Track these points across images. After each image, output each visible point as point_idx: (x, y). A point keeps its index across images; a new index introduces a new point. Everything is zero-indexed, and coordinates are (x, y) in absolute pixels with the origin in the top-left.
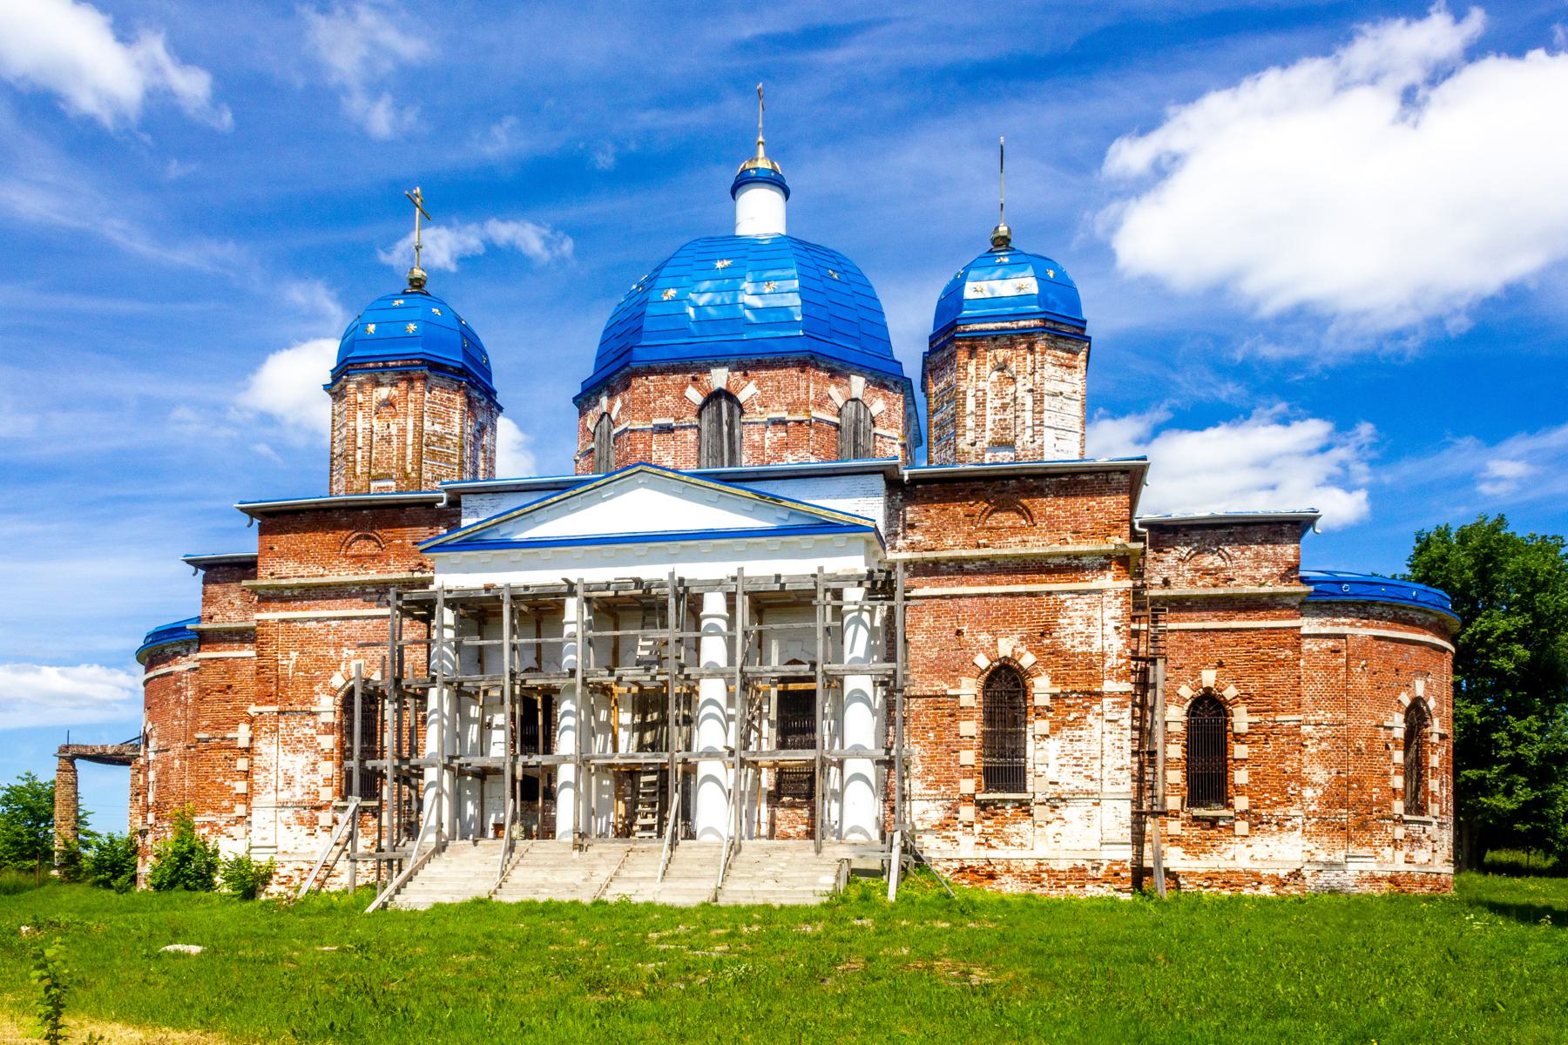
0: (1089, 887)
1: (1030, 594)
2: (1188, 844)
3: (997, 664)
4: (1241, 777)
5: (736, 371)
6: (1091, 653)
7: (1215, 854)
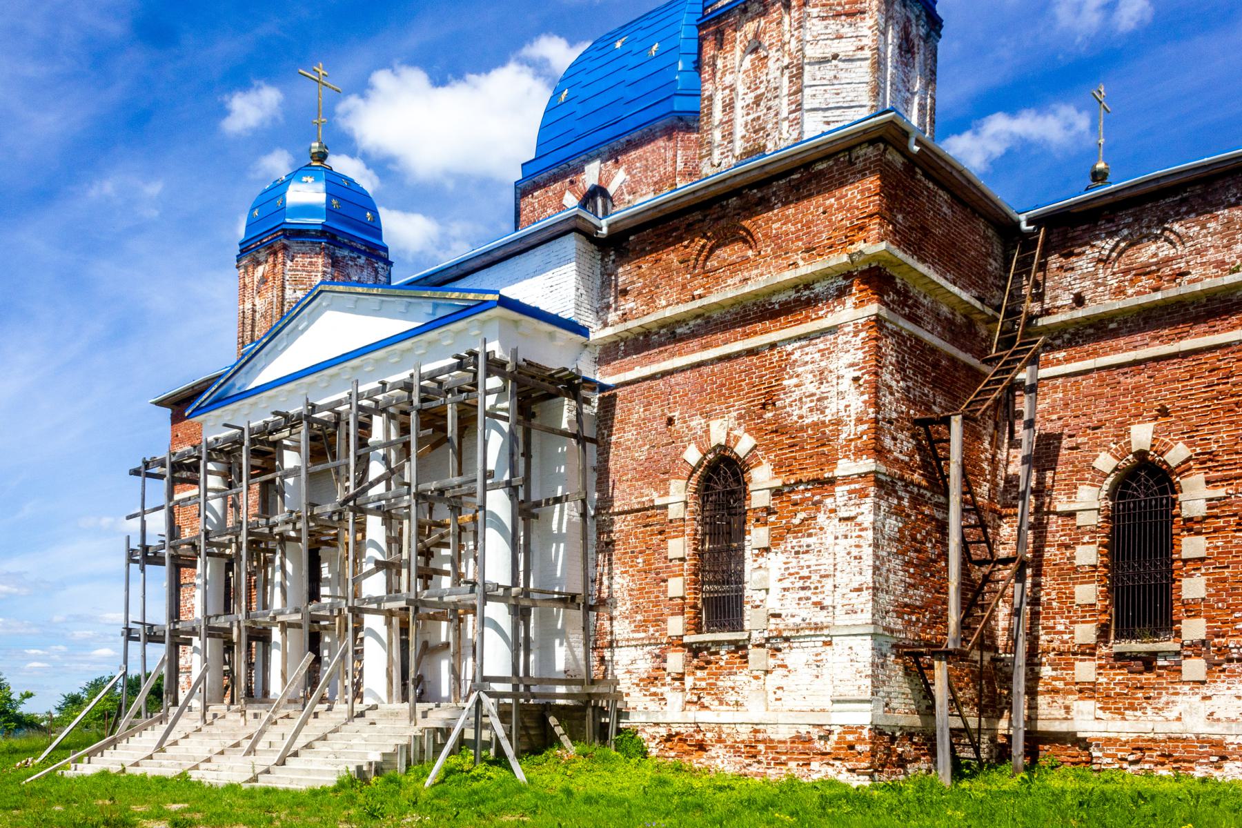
0: (815, 765)
1: (751, 352)
2: (1108, 696)
3: (711, 456)
4: (1193, 587)
5: (607, 160)
6: (823, 422)
7: (1149, 711)
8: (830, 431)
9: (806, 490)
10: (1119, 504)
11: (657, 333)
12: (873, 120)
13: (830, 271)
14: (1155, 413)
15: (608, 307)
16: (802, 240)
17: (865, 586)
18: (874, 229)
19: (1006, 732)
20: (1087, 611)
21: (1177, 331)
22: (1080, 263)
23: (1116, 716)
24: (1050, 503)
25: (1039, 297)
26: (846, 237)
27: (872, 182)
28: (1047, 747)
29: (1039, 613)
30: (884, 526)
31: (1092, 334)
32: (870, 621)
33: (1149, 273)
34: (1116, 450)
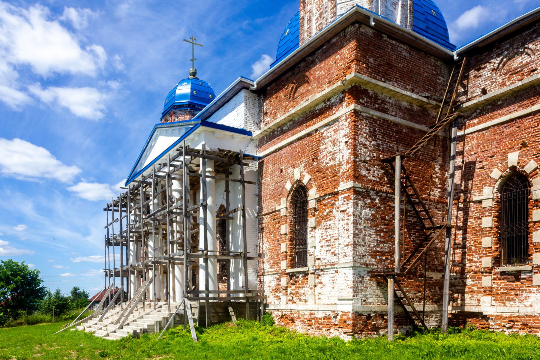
0: (332, 330)
1: (309, 135)
3: (295, 186)
7: (517, 301)
8: (337, 169)
9: (329, 198)
10: (504, 195)
11: (277, 131)
12: (348, 12)
13: (335, 91)
14: (520, 146)
15: (261, 121)
16: (327, 78)
17: (350, 243)
18: (353, 67)
19: (450, 312)
20: (488, 251)
21: (530, 101)
22: (484, 72)
23: (501, 304)
24: (470, 197)
25: (465, 93)
26: (344, 73)
27: (353, 44)
28: (470, 320)
29: (465, 252)
30: (361, 214)
31: (490, 109)
32: (352, 261)
33: (517, 72)
34: (501, 167)
